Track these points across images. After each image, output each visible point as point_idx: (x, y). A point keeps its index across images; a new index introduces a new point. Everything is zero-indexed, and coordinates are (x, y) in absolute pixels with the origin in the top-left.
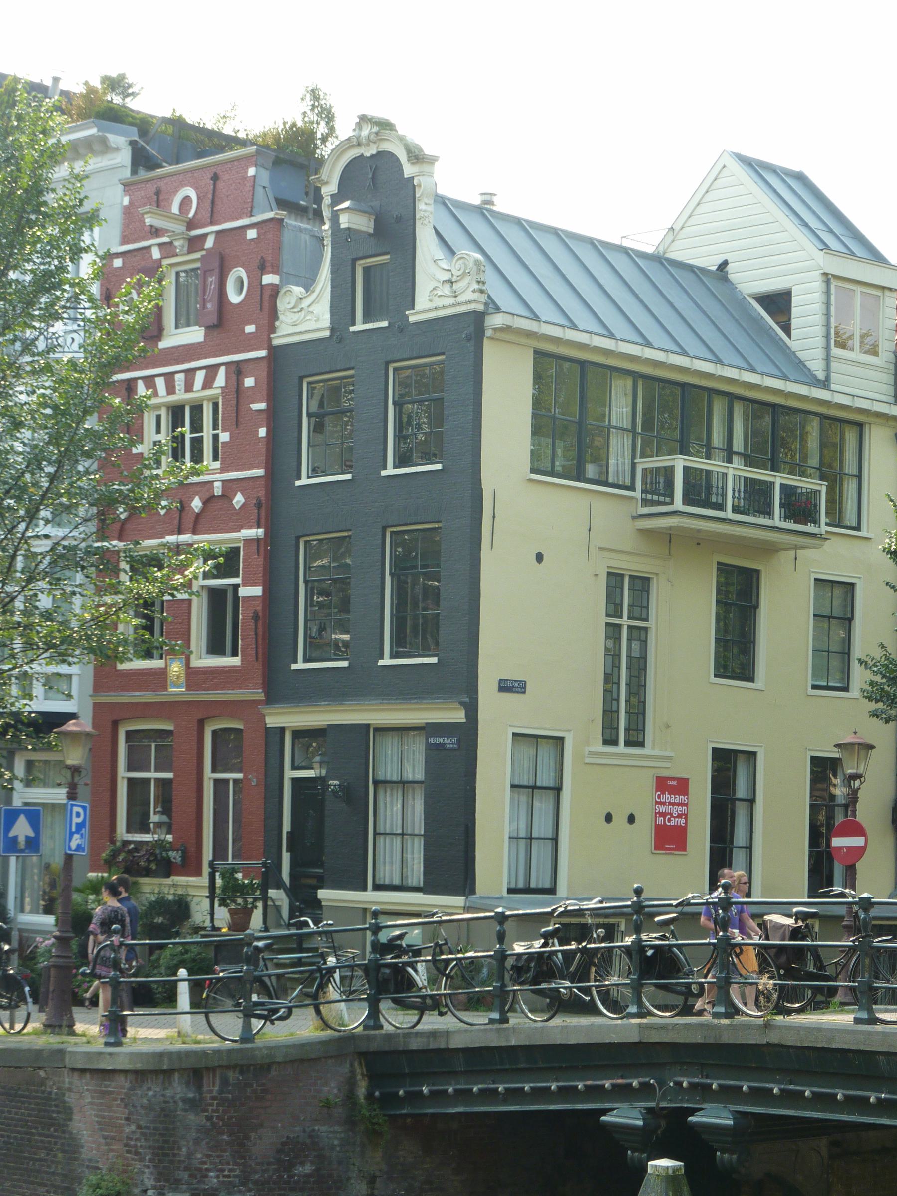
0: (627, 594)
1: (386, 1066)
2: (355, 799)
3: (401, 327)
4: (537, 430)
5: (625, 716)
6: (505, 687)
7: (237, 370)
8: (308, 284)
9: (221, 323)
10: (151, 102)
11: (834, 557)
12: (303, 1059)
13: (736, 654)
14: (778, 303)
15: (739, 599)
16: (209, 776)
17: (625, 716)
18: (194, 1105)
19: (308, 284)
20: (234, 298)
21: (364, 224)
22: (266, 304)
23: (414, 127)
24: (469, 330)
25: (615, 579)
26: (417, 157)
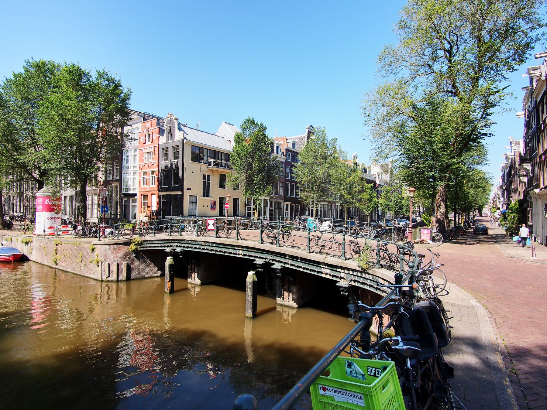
0: (206, 178)
5: (206, 193)
6: (188, 189)
13: (222, 186)
15: (223, 178)
16: (143, 201)
17: (206, 193)
25: (204, 176)
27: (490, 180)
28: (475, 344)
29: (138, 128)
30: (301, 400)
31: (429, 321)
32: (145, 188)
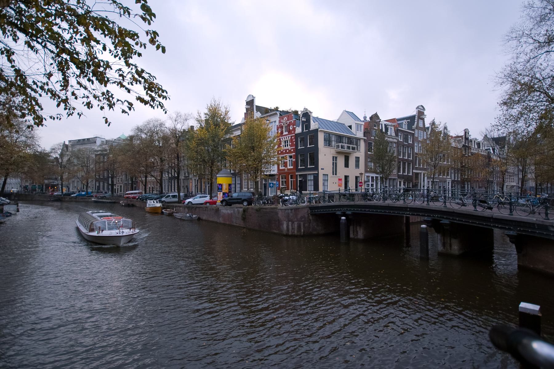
0: (335, 159)
1: (312, 208)
2: (306, 182)
3: (309, 131)
4: (325, 140)
5: (335, 172)
7: (291, 137)
9: (289, 132)
10: (280, 109)
11: (357, 154)
12: (303, 208)
13: (347, 165)
14: (350, 127)
17: (335, 172)
18: (291, 213)
20: (291, 129)
21: (305, 120)
22: (294, 129)
23: (310, 109)
24: (316, 131)
25: (333, 157)
26: (311, 113)
27: (203, 118)
28: (505, 208)
29: (275, 122)
32: (284, 170)
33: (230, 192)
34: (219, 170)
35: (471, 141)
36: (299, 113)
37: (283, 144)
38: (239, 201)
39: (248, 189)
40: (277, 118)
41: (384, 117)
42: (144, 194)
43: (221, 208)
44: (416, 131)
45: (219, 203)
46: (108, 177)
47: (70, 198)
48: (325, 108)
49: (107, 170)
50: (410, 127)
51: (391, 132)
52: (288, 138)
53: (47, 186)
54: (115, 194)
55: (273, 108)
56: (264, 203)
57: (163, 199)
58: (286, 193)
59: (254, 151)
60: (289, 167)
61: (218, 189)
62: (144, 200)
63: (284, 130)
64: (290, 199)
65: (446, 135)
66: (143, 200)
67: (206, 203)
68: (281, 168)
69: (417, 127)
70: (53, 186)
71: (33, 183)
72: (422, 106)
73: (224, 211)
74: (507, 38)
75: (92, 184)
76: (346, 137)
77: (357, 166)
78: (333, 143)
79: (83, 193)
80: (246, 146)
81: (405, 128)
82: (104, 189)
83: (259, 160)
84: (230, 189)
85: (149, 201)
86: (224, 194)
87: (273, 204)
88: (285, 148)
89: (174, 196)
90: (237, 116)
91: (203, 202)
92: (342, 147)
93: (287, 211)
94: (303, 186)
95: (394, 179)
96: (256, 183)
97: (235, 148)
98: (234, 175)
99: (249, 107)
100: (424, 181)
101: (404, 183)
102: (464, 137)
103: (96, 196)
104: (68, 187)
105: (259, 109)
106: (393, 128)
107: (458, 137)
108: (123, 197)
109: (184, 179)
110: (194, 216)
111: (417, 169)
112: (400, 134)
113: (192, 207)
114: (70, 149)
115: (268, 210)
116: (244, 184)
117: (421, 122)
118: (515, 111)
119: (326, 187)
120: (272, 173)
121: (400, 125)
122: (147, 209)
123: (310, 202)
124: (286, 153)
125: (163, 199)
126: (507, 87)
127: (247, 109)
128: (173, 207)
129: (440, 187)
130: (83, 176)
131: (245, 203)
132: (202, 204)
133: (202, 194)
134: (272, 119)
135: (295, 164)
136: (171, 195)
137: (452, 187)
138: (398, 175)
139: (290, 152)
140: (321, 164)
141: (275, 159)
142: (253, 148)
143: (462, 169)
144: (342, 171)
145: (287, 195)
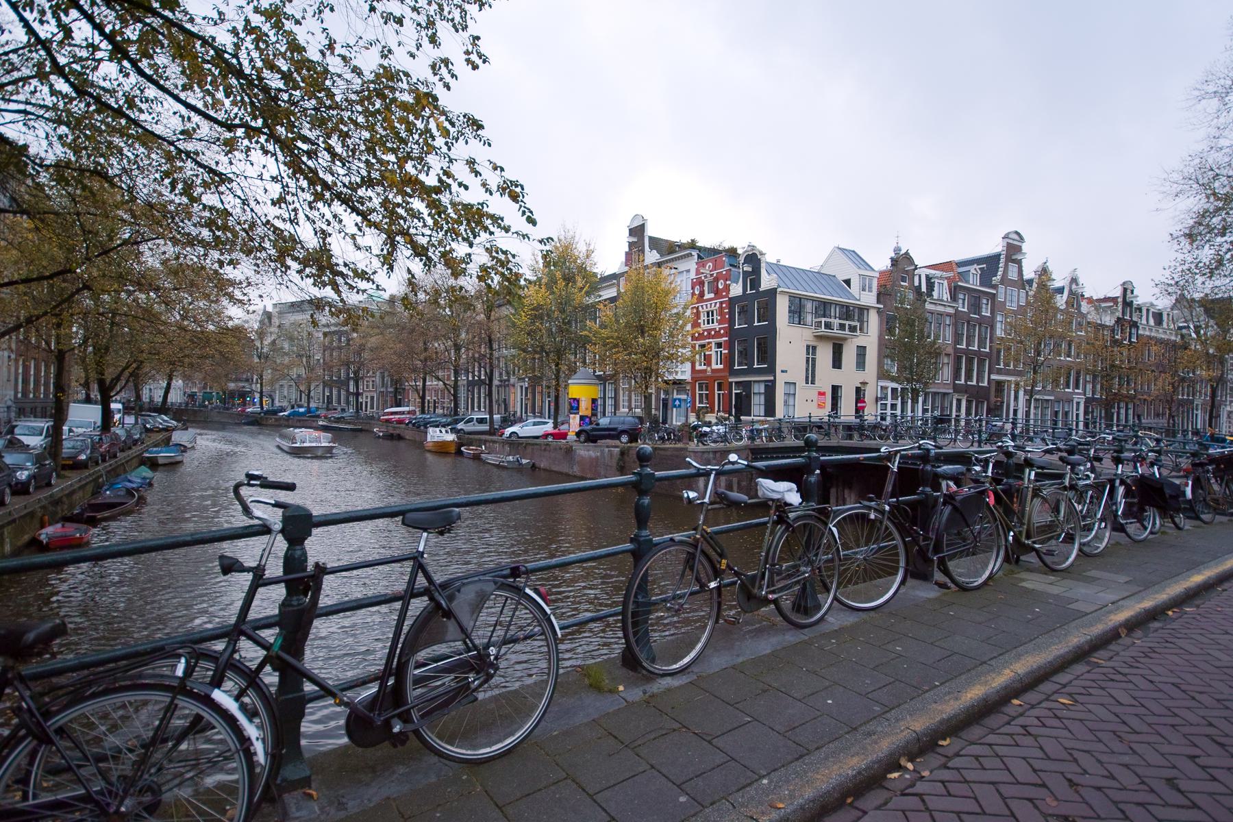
0: (811, 350)
2: (748, 397)
3: (758, 292)
5: (811, 378)
7: (721, 303)
8: (737, 283)
9: (717, 293)
11: (861, 340)
13: (837, 363)
14: (848, 282)
17: (811, 378)
19: (737, 283)
22: (727, 288)
23: (760, 247)
24: (773, 293)
25: (808, 347)
26: (762, 254)
30: (617, 589)
31: (494, 748)
32: (705, 371)
33: (594, 415)
34: (573, 371)
35: (1139, 309)
36: (740, 251)
37: (703, 317)
38: (612, 433)
39: (630, 409)
40: (691, 264)
41: (924, 257)
42: (418, 415)
43: (576, 446)
44: (1001, 289)
45: (571, 436)
46: (348, 379)
47: (276, 420)
48: (794, 242)
49: (347, 364)
50: (986, 278)
51: (942, 292)
52: (714, 306)
53: (232, 394)
54: (362, 413)
55: (684, 241)
56: (662, 438)
57: (460, 426)
58: (707, 419)
59: (643, 333)
60: (714, 366)
61: (572, 408)
62: (421, 427)
63: (706, 288)
64: (712, 432)
65: (1076, 297)
66: (419, 427)
67: (546, 436)
68: (698, 367)
69: (1004, 280)
70: (243, 395)
71: (205, 388)
72: (1017, 233)
73: (582, 453)
74: (1197, 93)
75: (317, 392)
76: (836, 304)
77: (861, 364)
78: (809, 318)
79: (302, 410)
80: (627, 325)
81: (974, 282)
82: (339, 403)
83: (654, 353)
84: (594, 409)
85: (431, 430)
86: (582, 418)
87: (679, 441)
88: (706, 326)
89: (481, 421)
90: (608, 257)
91: (540, 434)
92: (828, 326)
93: (706, 455)
94: (743, 406)
95: (945, 394)
96: (648, 398)
97: (606, 327)
98: (603, 380)
99: (635, 240)
100: (1016, 398)
101: (969, 402)
102: (1120, 300)
103: (326, 417)
104: (271, 396)
105: (656, 243)
106: (945, 283)
107: (1106, 299)
108: (379, 419)
109: (498, 386)
110: (524, 461)
111: (999, 372)
112: (961, 296)
113: (517, 444)
114: (276, 321)
115: (669, 453)
116: (623, 398)
117: (1013, 269)
118: (1206, 254)
119: (791, 409)
120: (679, 377)
121: (963, 276)
122: (429, 446)
123: (752, 438)
124: (709, 336)
125: (460, 426)
126: (1194, 202)
127: (631, 244)
128: (480, 443)
129: (1056, 413)
130: (299, 376)
131: (624, 438)
132: (537, 437)
133: (535, 417)
134: (682, 266)
135: (728, 361)
136: (475, 417)
137: (1086, 413)
138: (955, 384)
139: (718, 335)
140: (782, 360)
141: (687, 352)
142: (642, 330)
143: (1106, 375)
144: (826, 375)
145: (709, 424)
